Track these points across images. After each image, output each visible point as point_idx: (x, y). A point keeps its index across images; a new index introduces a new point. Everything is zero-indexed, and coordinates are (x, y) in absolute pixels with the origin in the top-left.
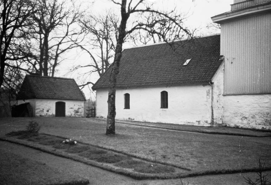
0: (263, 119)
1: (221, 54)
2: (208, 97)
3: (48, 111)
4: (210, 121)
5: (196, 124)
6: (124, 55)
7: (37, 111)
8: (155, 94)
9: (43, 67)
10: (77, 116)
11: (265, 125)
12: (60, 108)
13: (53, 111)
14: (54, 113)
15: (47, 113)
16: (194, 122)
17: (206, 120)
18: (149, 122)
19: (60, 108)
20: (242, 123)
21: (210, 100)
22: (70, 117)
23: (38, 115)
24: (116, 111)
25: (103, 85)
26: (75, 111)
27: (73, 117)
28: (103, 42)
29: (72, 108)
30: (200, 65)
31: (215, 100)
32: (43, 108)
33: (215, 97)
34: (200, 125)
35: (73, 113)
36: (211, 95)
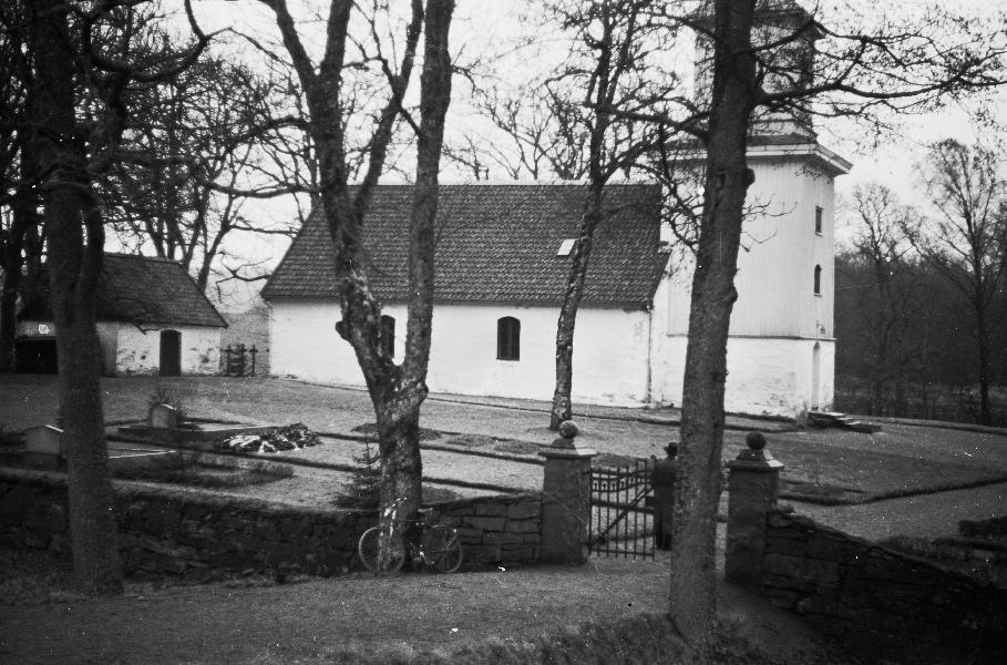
0: (765, 392)
1: (662, 239)
2: (638, 338)
3: (143, 357)
4: (641, 395)
5: (606, 402)
6: (376, 199)
7: (120, 358)
8: (486, 321)
9: (85, 243)
10: (205, 372)
11: (769, 404)
12: (171, 347)
13: (154, 361)
14: (157, 364)
15: (141, 362)
16: (599, 396)
17: (630, 393)
18: (523, 397)
19: (171, 347)
20: (207, 369)
21: (644, 346)
22: (191, 375)
23: (122, 368)
24: (685, 351)
25: (304, 290)
26: (201, 356)
27: (196, 375)
28: (279, 168)
29: (194, 349)
30: (608, 259)
31: (654, 349)
32: (134, 349)
33: (655, 338)
34: (613, 404)
35: (663, 456)
36: (646, 334)
